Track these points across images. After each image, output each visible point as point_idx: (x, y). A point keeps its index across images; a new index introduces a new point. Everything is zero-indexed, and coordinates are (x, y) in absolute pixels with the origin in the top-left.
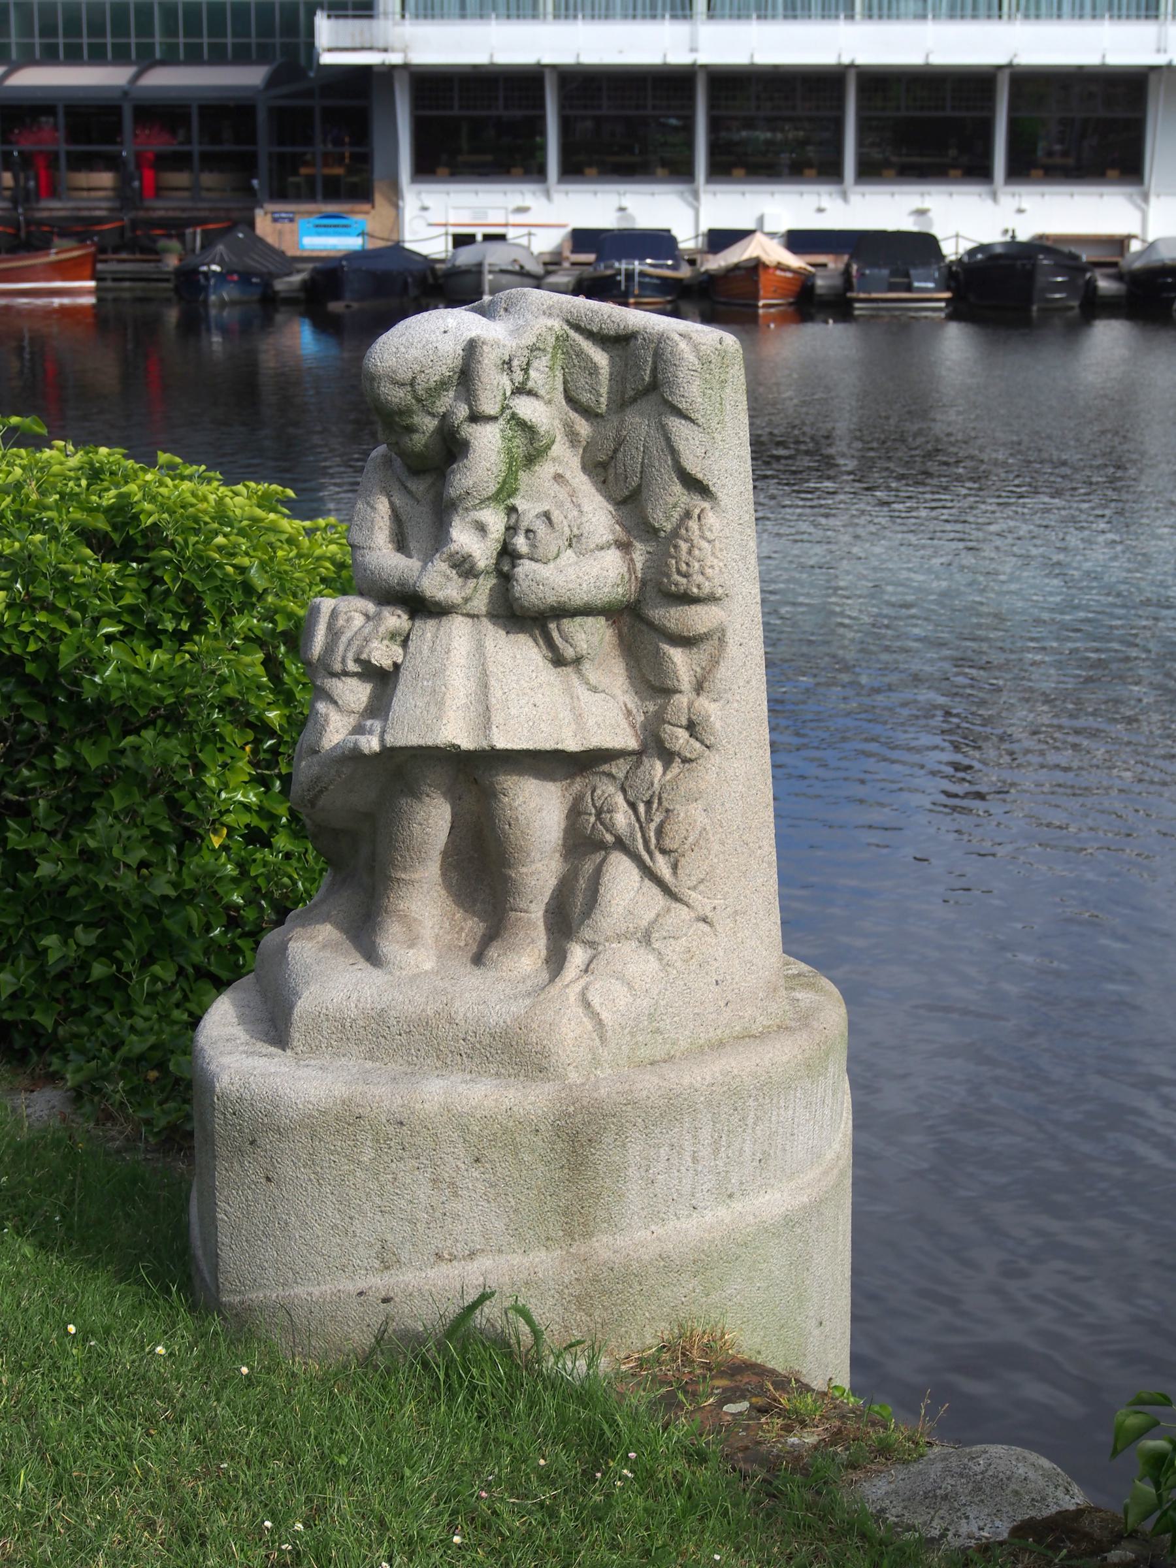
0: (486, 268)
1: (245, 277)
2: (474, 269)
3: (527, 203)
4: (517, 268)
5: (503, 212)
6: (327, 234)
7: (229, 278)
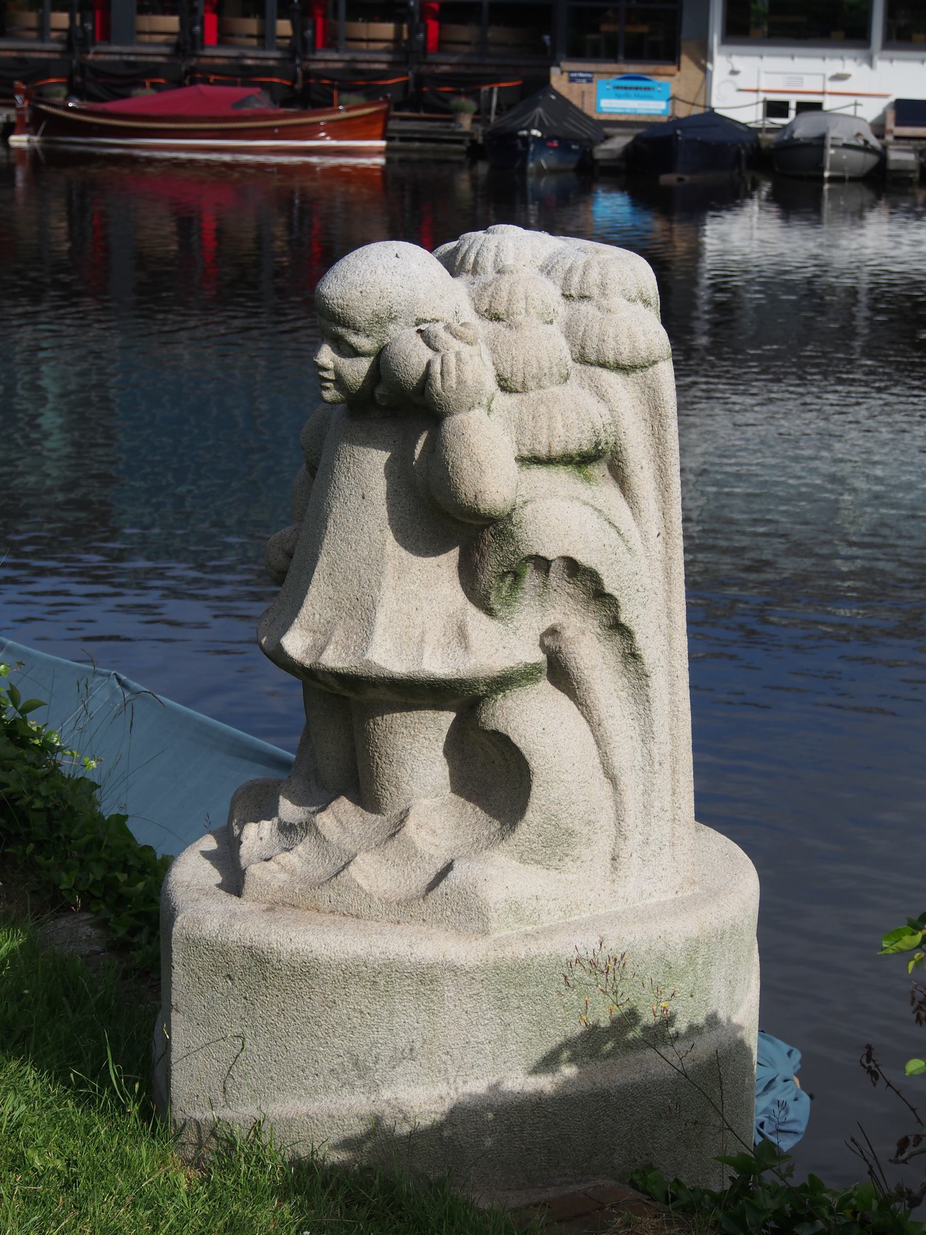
0: (829, 142)
1: (565, 144)
2: (815, 142)
3: (846, 71)
4: (861, 143)
5: (821, 78)
6: (627, 97)
7: (549, 144)
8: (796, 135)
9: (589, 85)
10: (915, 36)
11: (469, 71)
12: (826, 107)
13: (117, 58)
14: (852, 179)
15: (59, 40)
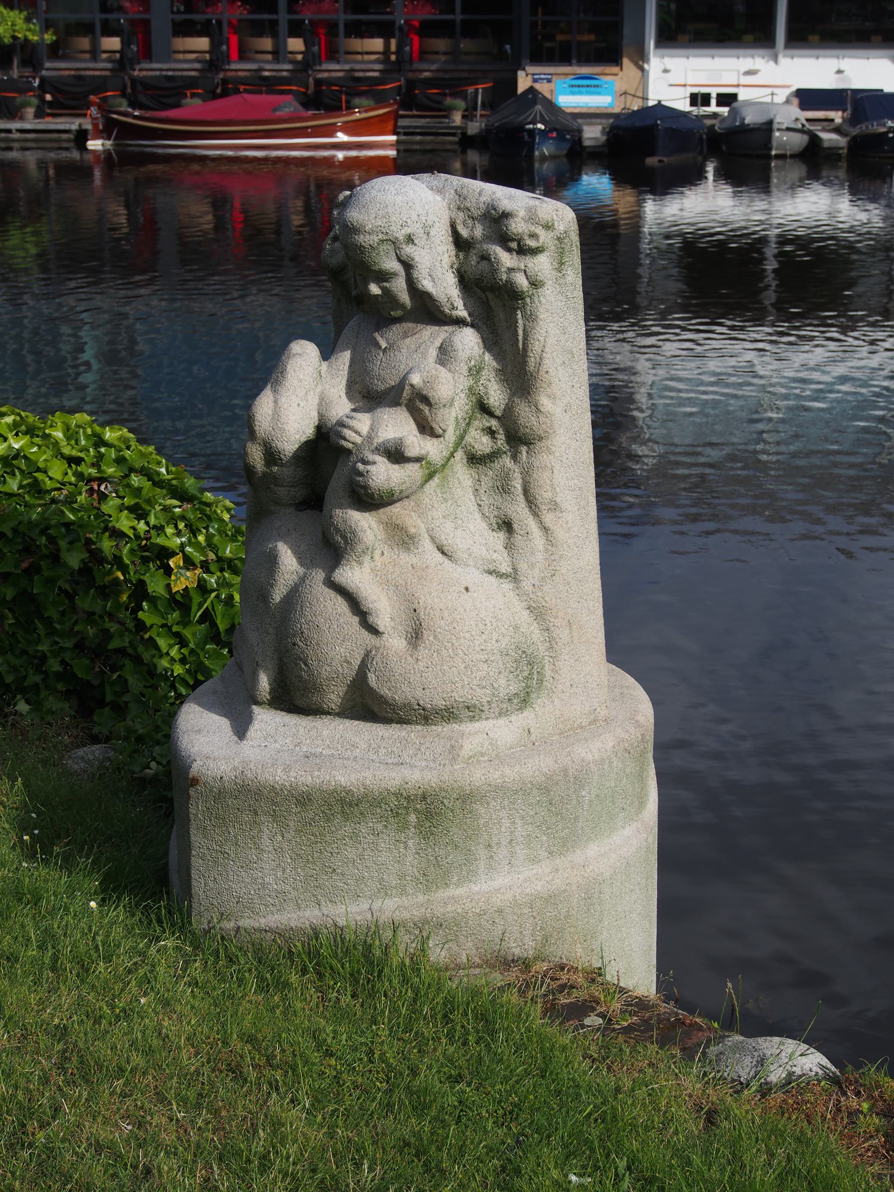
0: (775, 126)
2: (763, 127)
3: (756, 67)
4: (800, 126)
5: (736, 73)
6: (580, 93)
7: (550, 135)
8: (747, 121)
9: (549, 85)
10: (810, 38)
11: (447, 76)
12: (741, 98)
13: (158, 73)
14: (792, 156)
15: (109, 60)
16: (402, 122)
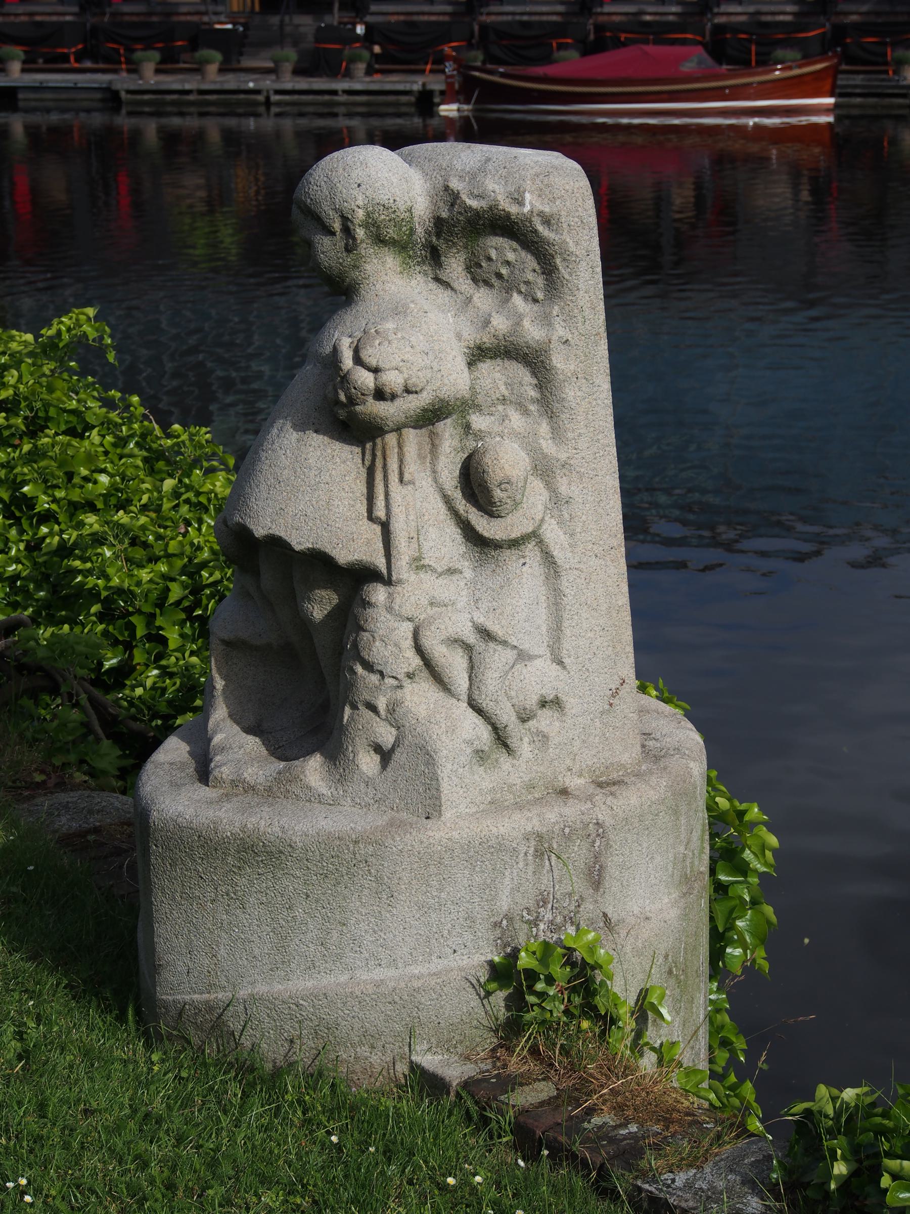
11: (880, 20)
13: (510, 18)
16: (842, 80)
